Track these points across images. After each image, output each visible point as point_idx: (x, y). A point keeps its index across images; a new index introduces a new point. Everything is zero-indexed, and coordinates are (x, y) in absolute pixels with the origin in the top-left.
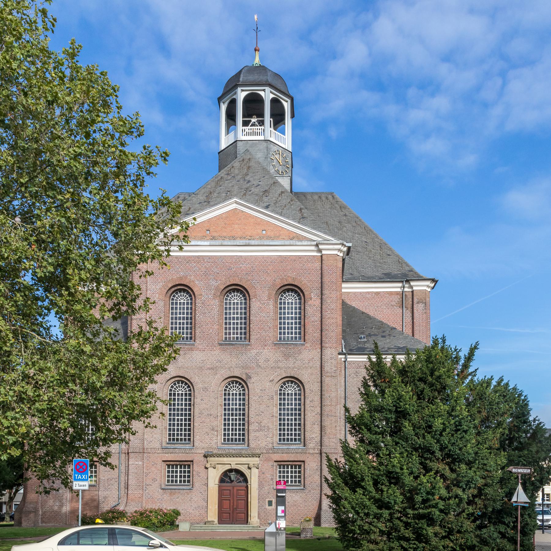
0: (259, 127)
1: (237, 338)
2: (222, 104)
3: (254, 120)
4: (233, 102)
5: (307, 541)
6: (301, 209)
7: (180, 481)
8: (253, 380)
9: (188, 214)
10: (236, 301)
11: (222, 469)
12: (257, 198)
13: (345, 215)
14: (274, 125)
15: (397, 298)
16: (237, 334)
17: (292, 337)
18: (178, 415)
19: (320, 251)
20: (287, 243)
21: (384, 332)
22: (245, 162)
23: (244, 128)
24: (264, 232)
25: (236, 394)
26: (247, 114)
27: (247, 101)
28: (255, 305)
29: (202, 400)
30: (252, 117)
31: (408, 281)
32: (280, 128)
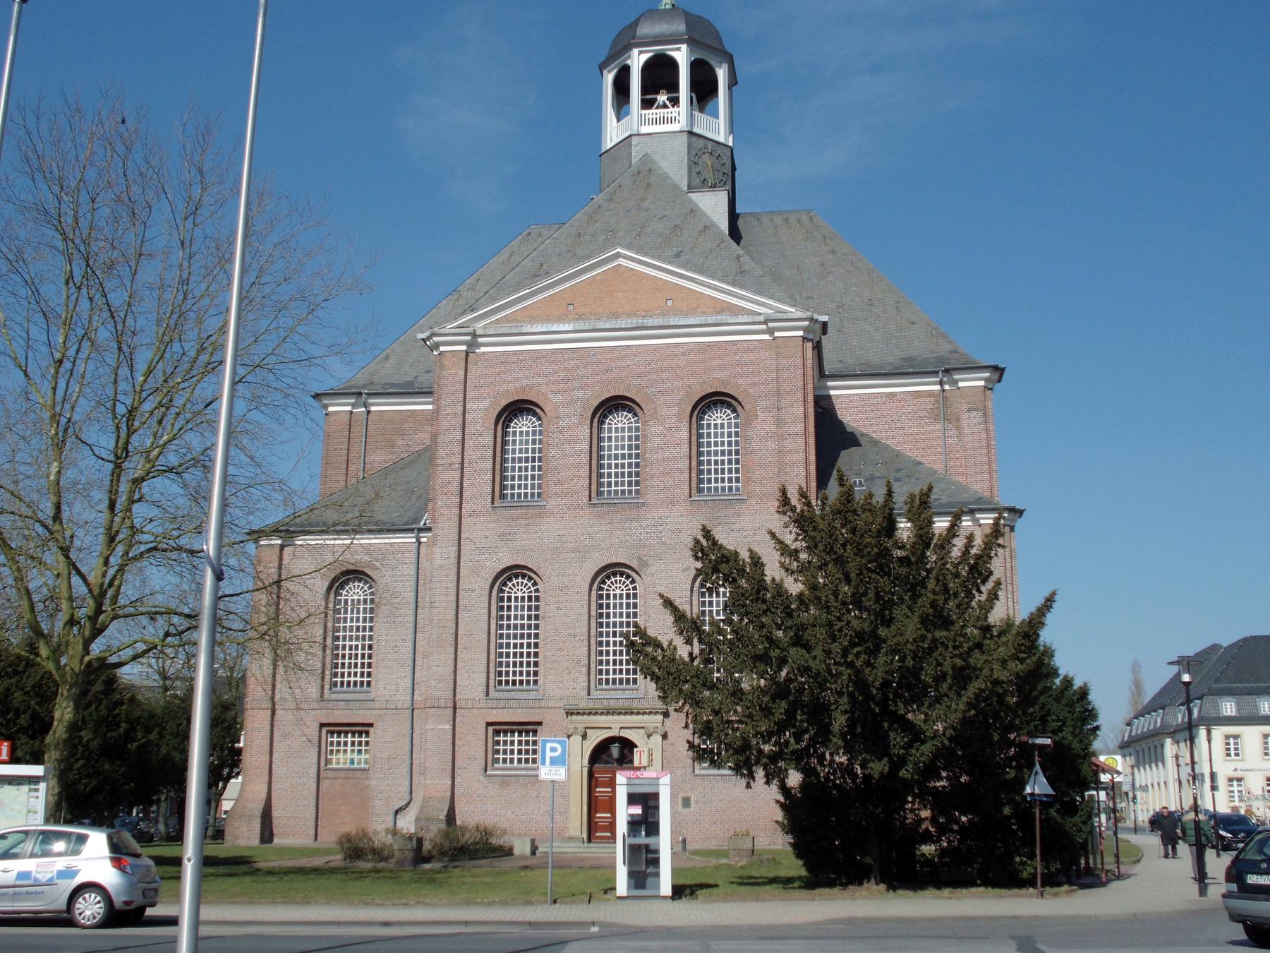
0: (671, 109)
1: (623, 492)
2: (605, 72)
3: (662, 98)
4: (624, 73)
5: (809, 869)
6: (738, 257)
7: (520, 761)
8: (651, 569)
9: (537, 276)
10: (620, 425)
11: (596, 738)
12: (660, 240)
13: (833, 252)
14: (699, 101)
15: (928, 404)
16: (623, 484)
17: (723, 489)
18: (515, 637)
19: (770, 331)
20: (710, 320)
21: (898, 470)
22: (642, 176)
23: (643, 112)
24: (669, 303)
25: (621, 596)
26: (650, 88)
27: (648, 68)
28: (655, 431)
29: (558, 608)
30: (658, 93)
31: (947, 371)
32: (710, 105)
